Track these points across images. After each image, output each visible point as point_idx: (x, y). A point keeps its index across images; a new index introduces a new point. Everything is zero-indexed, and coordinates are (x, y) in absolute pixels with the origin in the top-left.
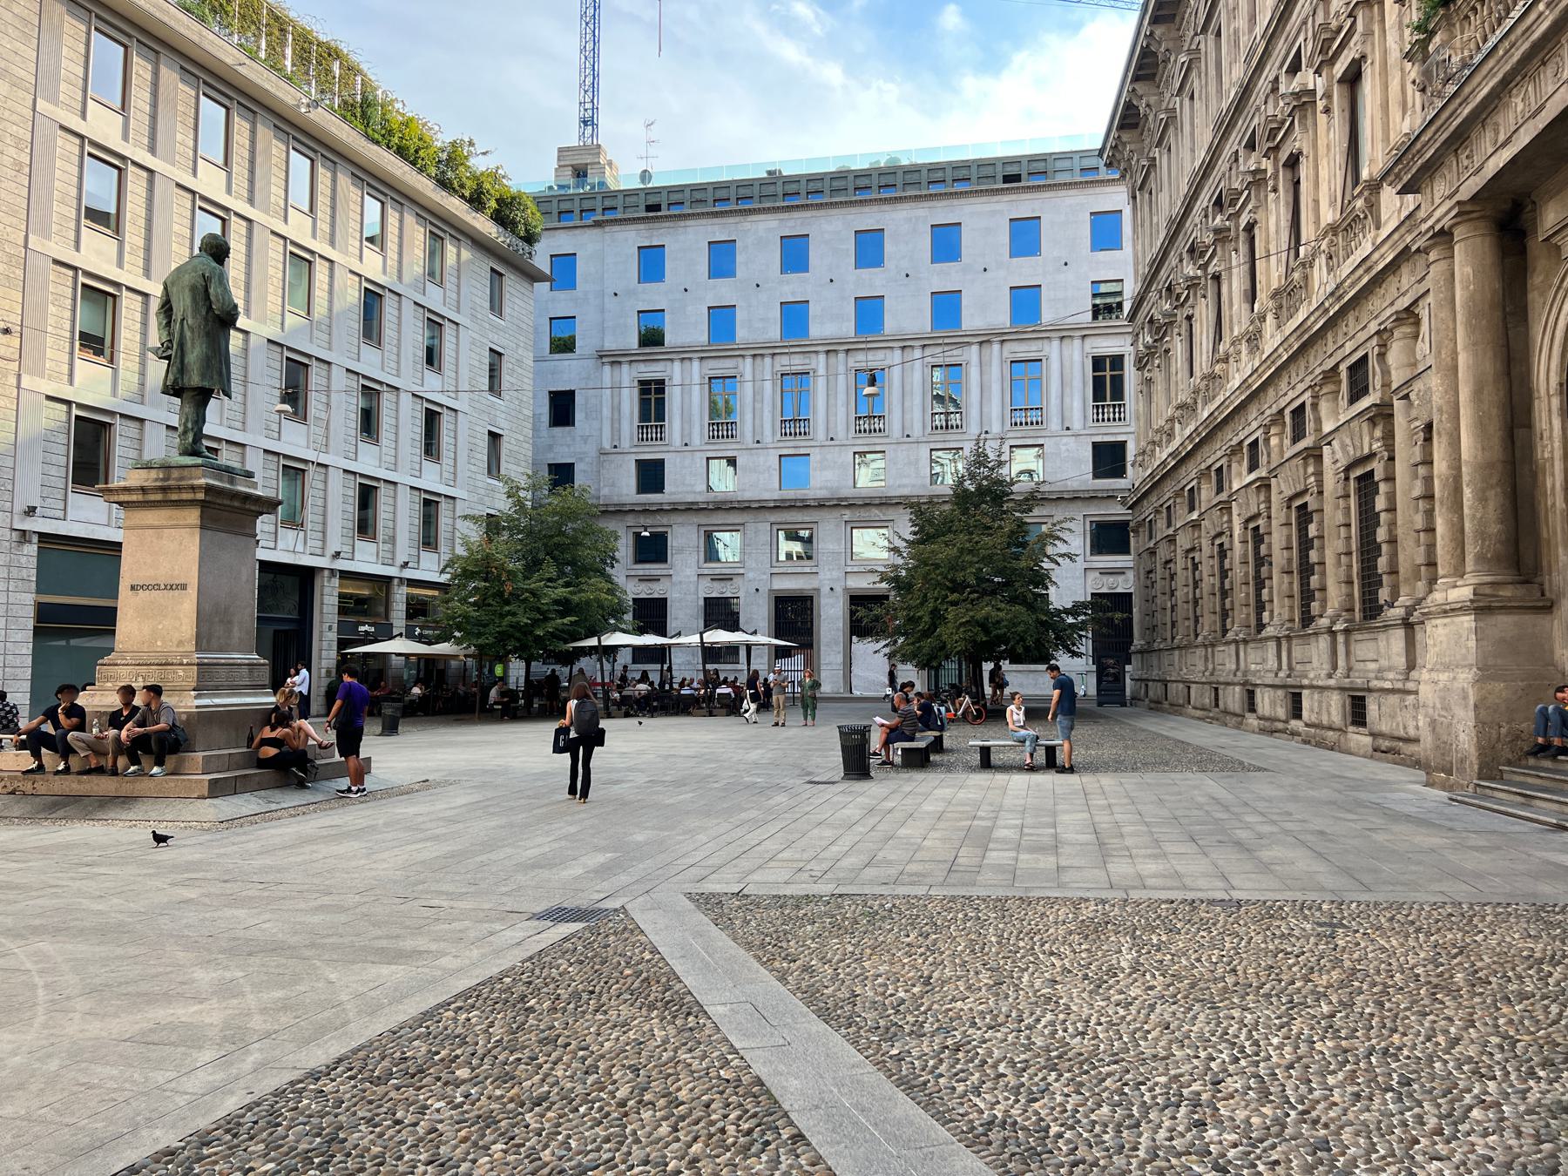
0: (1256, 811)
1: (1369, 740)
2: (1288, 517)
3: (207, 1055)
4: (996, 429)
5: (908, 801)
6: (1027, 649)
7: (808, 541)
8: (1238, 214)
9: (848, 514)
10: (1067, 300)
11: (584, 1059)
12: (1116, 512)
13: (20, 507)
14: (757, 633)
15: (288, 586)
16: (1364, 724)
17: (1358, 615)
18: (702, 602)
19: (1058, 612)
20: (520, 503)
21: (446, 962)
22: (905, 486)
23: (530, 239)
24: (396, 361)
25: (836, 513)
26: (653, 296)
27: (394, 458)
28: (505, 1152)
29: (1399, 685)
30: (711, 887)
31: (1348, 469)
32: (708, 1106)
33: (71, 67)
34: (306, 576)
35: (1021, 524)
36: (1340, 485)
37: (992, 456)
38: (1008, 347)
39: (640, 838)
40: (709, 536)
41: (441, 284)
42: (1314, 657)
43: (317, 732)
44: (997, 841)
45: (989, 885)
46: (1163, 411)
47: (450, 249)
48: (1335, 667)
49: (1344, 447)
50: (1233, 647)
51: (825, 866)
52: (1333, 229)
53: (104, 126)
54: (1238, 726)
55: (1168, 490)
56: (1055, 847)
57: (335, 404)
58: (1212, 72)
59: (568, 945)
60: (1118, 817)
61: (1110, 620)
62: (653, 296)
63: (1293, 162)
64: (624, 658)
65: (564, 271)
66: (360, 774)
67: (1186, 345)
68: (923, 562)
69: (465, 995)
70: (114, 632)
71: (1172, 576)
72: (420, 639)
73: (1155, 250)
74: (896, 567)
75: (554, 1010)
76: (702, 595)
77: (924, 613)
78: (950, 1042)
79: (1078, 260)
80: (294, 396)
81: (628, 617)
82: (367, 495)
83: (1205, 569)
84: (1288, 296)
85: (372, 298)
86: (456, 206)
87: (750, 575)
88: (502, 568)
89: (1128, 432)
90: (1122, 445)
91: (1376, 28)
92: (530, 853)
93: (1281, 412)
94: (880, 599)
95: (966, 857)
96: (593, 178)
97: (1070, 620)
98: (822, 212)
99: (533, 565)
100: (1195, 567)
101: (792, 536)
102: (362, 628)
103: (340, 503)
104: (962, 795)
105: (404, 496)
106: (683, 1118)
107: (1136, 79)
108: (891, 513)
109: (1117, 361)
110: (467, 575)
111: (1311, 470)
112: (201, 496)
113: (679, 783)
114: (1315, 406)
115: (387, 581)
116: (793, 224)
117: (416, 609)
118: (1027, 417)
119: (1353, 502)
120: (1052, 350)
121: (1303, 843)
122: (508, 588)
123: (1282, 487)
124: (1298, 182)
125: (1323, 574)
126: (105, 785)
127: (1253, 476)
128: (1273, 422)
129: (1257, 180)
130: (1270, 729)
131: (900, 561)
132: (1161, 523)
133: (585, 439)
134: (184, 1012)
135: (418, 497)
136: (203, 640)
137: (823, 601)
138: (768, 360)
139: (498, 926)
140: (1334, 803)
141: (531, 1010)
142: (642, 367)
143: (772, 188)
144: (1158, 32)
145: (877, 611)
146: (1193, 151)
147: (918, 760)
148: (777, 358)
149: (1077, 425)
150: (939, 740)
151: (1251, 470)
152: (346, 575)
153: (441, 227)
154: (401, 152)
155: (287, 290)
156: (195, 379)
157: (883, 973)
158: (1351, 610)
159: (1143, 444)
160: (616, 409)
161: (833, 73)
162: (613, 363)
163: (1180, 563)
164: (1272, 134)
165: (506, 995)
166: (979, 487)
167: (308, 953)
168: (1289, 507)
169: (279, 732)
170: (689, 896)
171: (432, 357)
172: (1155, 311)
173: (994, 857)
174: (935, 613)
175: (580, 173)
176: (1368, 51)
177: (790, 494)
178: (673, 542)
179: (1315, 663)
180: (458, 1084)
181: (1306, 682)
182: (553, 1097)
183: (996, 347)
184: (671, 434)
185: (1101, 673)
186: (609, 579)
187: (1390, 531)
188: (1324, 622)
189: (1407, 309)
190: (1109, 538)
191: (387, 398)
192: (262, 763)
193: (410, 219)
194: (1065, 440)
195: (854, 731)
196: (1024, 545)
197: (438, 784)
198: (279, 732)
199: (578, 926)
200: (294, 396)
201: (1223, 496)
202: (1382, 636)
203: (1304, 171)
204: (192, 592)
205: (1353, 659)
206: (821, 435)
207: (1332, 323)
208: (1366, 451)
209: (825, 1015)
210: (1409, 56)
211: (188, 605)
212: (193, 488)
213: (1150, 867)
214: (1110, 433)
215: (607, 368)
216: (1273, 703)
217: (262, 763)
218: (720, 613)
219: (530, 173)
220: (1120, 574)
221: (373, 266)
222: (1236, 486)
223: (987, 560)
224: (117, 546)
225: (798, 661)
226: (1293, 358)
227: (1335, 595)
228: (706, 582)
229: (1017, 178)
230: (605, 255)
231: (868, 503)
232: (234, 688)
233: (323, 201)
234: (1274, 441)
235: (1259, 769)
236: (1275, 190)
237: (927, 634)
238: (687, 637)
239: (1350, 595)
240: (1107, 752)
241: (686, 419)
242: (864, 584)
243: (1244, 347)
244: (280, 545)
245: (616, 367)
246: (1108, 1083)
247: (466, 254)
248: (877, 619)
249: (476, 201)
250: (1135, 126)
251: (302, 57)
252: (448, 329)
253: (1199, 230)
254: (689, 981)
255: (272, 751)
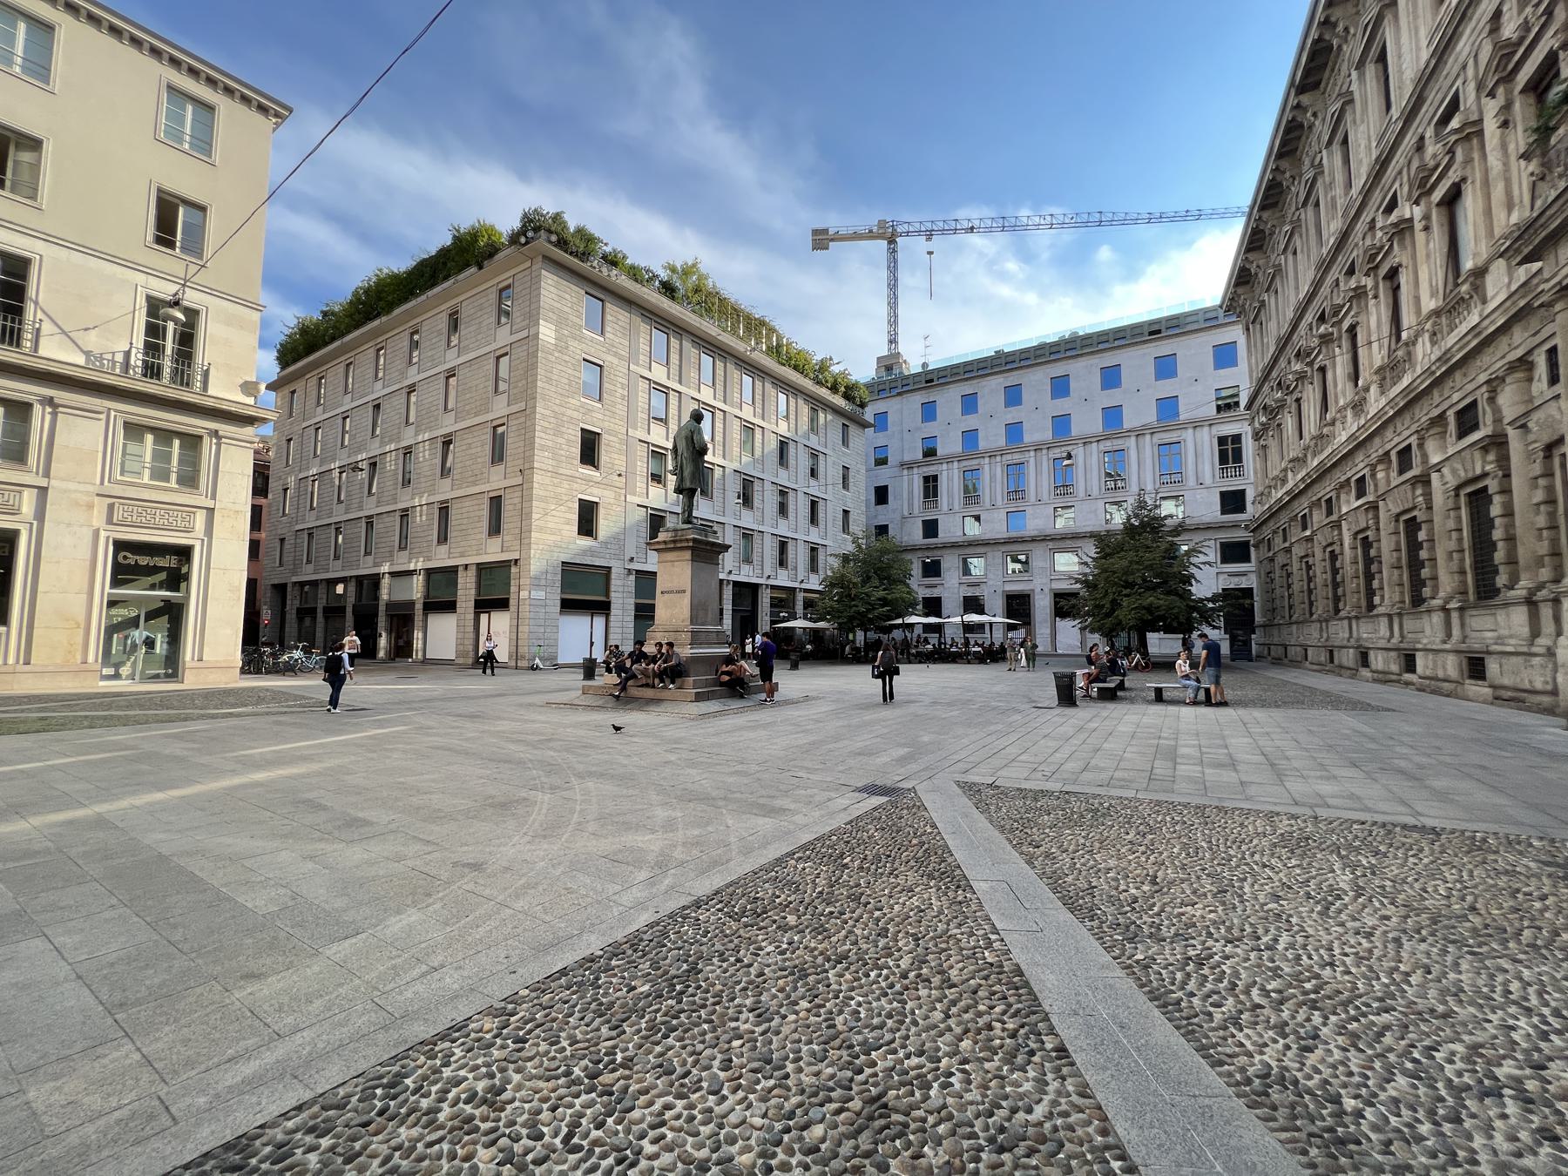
0: (1402, 744)
1: (1488, 691)
2: (1397, 528)
3: (643, 875)
4: (1149, 487)
5: (1106, 723)
6: (1180, 624)
7: (1026, 562)
8: (1341, 321)
9: (1051, 545)
10: (1197, 400)
11: (878, 920)
12: (1239, 535)
14: (995, 616)
15: (746, 593)
16: (1483, 678)
17: (1472, 597)
19: (1201, 600)
20: (859, 546)
21: (799, 819)
23: (862, 405)
24: (795, 477)
26: (930, 429)
27: (796, 527)
28: (808, 1011)
29: (1525, 649)
30: (973, 778)
31: (1458, 489)
32: (975, 992)
33: (644, 347)
34: (754, 588)
35: (1173, 544)
36: (1451, 501)
37: (1150, 502)
38: (1156, 436)
39: (926, 739)
40: (965, 561)
42: (1428, 630)
43: (750, 668)
44: (1183, 756)
45: (1183, 793)
46: (1276, 466)
47: (822, 416)
48: (1449, 635)
49: (1454, 472)
50: (1346, 622)
51: (1053, 768)
52: (1437, 313)
53: (659, 373)
54: (1353, 677)
55: (1283, 518)
56: (1232, 764)
57: (766, 499)
58: (1312, 231)
59: (876, 814)
60: (1278, 743)
61: (1236, 606)
62: (930, 429)
63: (1393, 274)
64: (918, 630)
65: (881, 421)
66: (772, 690)
67: (1295, 419)
68: (1104, 571)
69: (804, 848)
70: (653, 618)
71: (1289, 575)
72: (810, 620)
73: (1266, 361)
74: (1085, 575)
75: (861, 868)
77: (1106, 602)
78: (1192, 953)
79: (1199, 383)
80: (747, 499)
81: (920, 607)
82: (783, 546)
83: (1295, 579)
84: (1390, 371)
85: (783, 445)
86: (824, 392)
88: (850, 581)
89: (1249, 481)
90: (1243, 491)
91: (1476, 155)
92: (859, 745)
93: (1387, 453)
94: (1075, 595)
95: (1161, 768)
96: (896, 371)
97: (1210, 605)
99: (867, 580)
100: (1309, 567)
101: (1016, 560)
103: (769, 550)
104: (1145, 720)
105: (801, 545)
106: (954, 1003)
107: (1248, 250)
108: (1079, 543)
109: (1237, 438)
110: (832, 585)
111: (1419, 492)
113: (950, 704)
114: (1421, 446)
116: (1012, 379)
117: (808, 604)
118: (1172, 477)
119: (1464, 512)
120: (1188, 435)
121: (1470, 776)
122: (853, 592)
123: (1388, 509)
124: (1398, 287)
125: (1435, 566)
126: (649, 693)
127: (1360, 502)
128: (1380, 461)
129: (1359, 294)
130: (1383, 678)
131: (1088, 570)
132: (1278, 540)
133: (894, 511)
134: (639, 840)
135: (808, 547)
136: (694, 619)
139: (833, 795)
140: (1479, 740)
141: (845, 866)
144: (1265, 215)
145: (1073, 601)
146: (1297, 288)
147: (1109, 695)
149: (1208, 481)
150: (1122, 682)
151: (1358, 498)
152: (773, 587)
153: (817, 404)
154: (796, 368)
155: (743, 443)
156: (688, 484)
157: (1114, 867)
158: (1465, 593)
159: (1261, 489)
160: (911, 492)
161: (1031, 298)
163: (1296, 566)
164: (1372, 258)
165: (828, 851)
166: (1142, 522)
167: (721, 803)
168: (1397, 521)
169: (730, 668)
170: (958, 783)
171: (813, 473)
172: (1271, 403)
173: (1182, 769)
174: (1114, 602)
175: (889, 369)
176: (1468, 172)
177: (1014, 534)
179: (1428, 631)
180: (785, 928)
181: (1419, 646)
182: (853, 957)
183: (1148, 437)
185: (1233, 640)
186: (908, 586)
187: (1507, 531)
188: (1437, 602)
189: (1520, 359)
190: (1234, 552)
191: (791, 494)
192: (722, 684)
193: (801, 402)
195: (1064, 676)
196: (1175, 558)
197: (814, 698)
198: (730, 668)
199: (884, 799)
200: (747, 499)
201: (1334, 517)
202: (1499, 612)
203: (1404, 279)
205: (1468, 630)
207: (1438, 382)
208: (1478, 471)
209: (1071, 904)
210: (1526, 156)
211: (685, 601)
213: (1326, 788)
214: (1233, 485)
216: (1386, 661)
217: (722, 684)
218: (973, 604)
219: (863, 371)
220: (1247, 575)
221: (783, 428)
222: (1344, 510)
223: (1150, 568)
224: (655, 574)
225: (1021, 633)
226: (1399, 413)
227: (1447, 583)
228: (964, 588)
229: (1159, 332)
230: (903, 411)
231: (1063, 537)
232: (709, 644)
233: (758, 397)
234: (1380, 475)
235: (1388, 710)
236: (1376, 297)
237: (1108, 615)
238: (954, 619)
239: (1464, 582)
240: (1251, 693)
241: (951, 495)
242: (1064, 586)
243: (1349, 413)
244: (731, 568)
246: (1388, 1039)
247: (829, 417)
248: (1074, 606)
249: (834, 389)
250: (1247, 283)
251: (748, 328)
252: (821, 457)
253: (1305, 338)
254: (959, 856)
255: (727, 678)
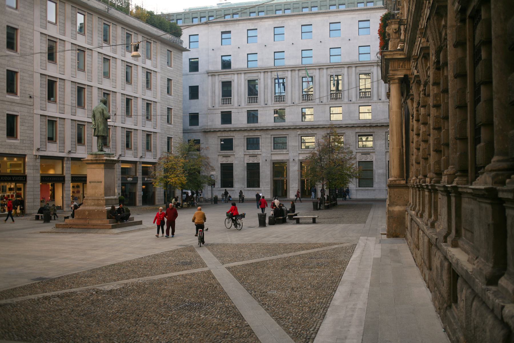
13: (35, 148)
18: (246, 165)
22: (321, 121)
25: (295, 131)
38: (358, 69)
41: (150, 59)
76: (246, 162)
87: (264, 155)
98: (289, 18)
102: (128, 179)
108: (315, 131)
112: (104, 162)
115: (135, 163)
137: (291, 164)
138: (269, 73)
142: (223, 77)
143: (271, 7)
148: (273, 73)
160: (213, 92)
162: (212, 75)
178: (235, 142)
183: (354, 69)
184: (234, 102)
194: (379, 104)
204: (103, 183)
206: (289, 102)
211: (102, 186)
212: (103, 160)
215: (210, 77)
228: (247, 157)
245: (213, 77)
